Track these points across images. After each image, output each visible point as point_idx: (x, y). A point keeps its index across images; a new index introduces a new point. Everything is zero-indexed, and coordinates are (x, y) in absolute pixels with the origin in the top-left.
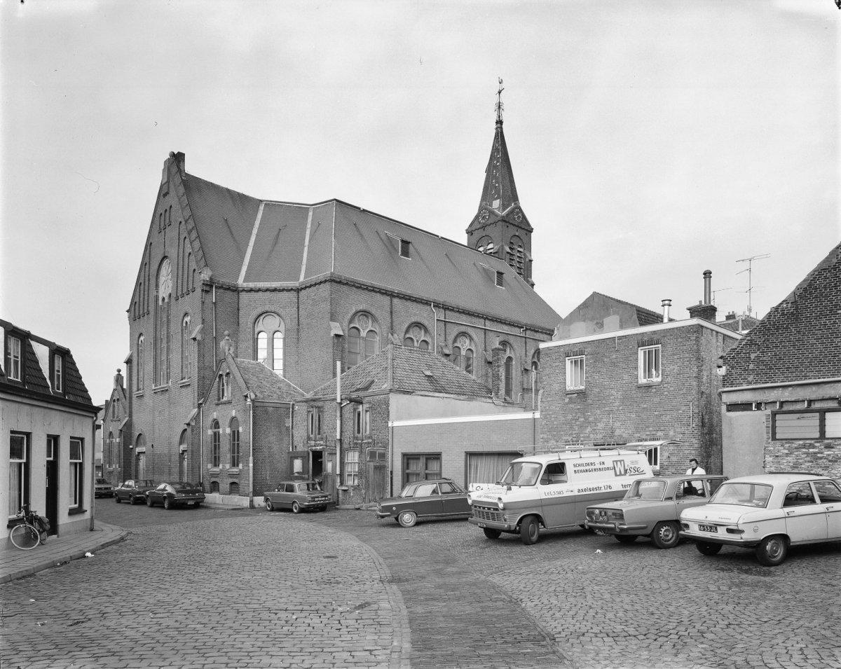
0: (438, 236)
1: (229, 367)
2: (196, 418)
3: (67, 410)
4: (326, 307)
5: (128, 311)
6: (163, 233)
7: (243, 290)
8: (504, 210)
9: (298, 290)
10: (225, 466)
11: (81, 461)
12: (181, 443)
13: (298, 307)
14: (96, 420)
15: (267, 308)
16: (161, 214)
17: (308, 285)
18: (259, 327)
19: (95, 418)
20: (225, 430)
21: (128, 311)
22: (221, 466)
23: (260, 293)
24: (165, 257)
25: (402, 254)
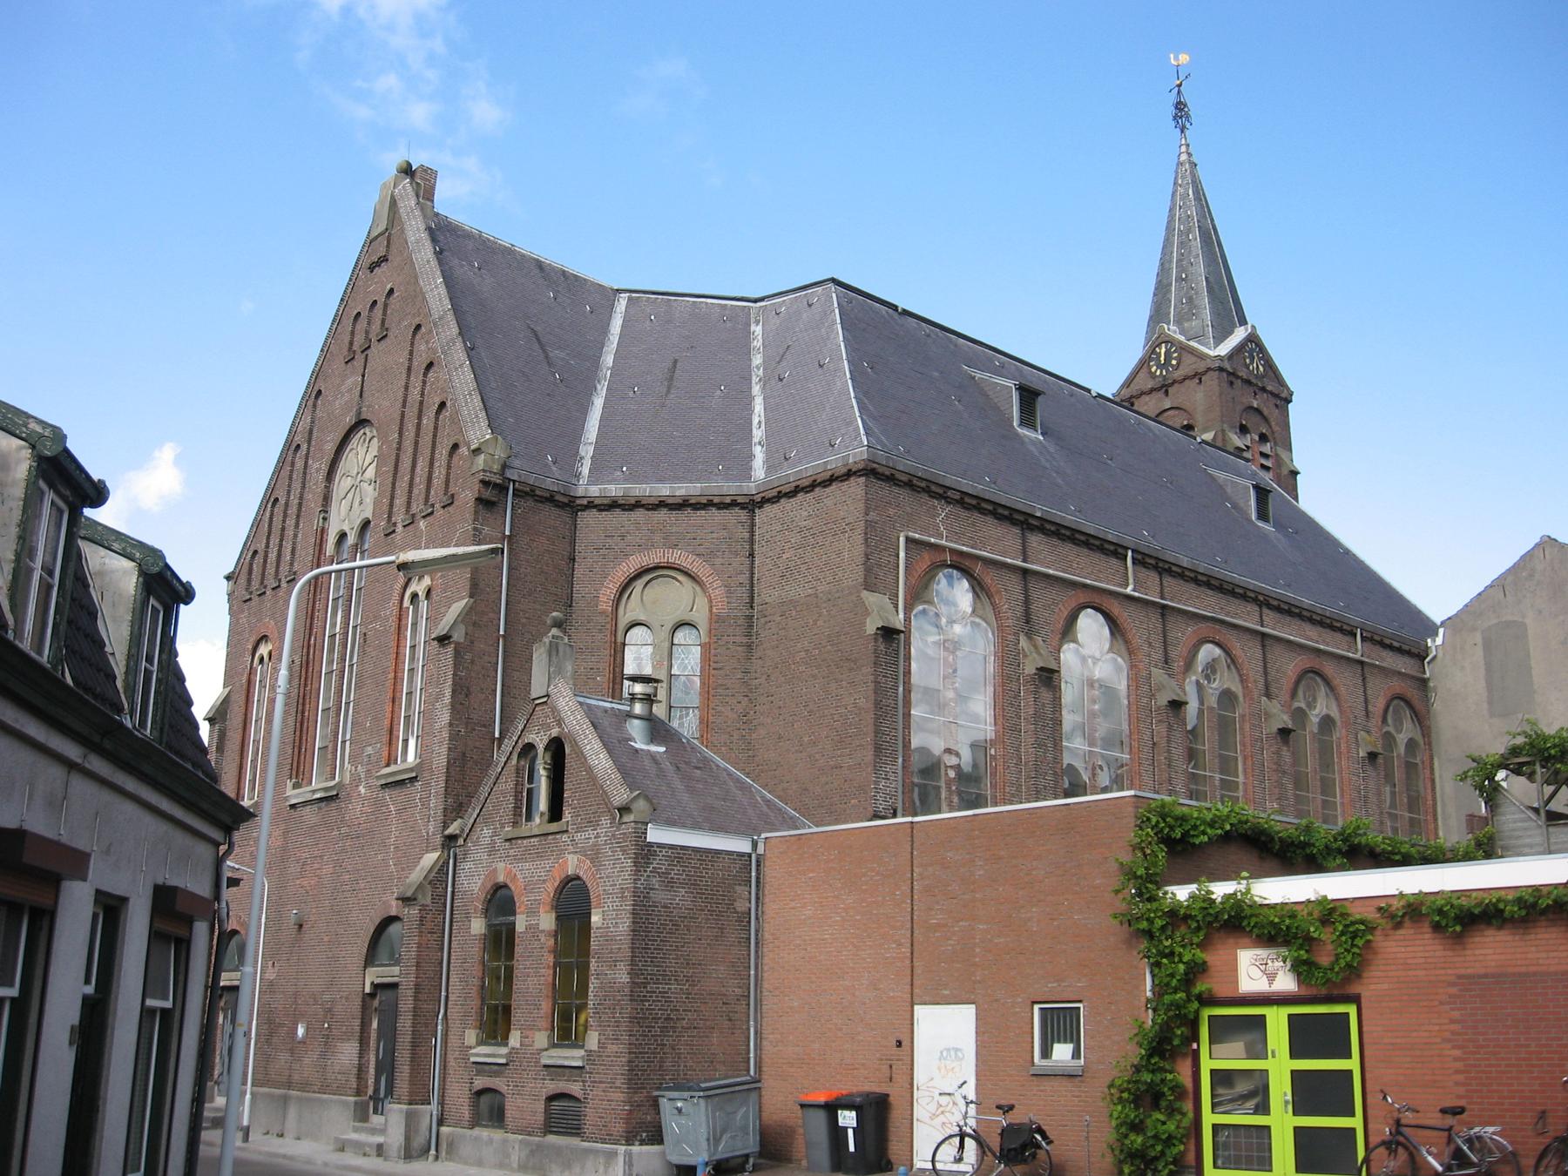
0: (1089, 391)
1: (560, 722)
2: (439, 876)
3: (165, 805)
4: (851, 548)
5: (228, 578)
6: (360, 358)
7: (591, 505)
8: (1220, 338)
9: (752, 505)
10: (531, 1036)
11: (168, 1004)
12: (370, 959)
13: (752, 555)
14: (228, 853)
15: (676, 556)
16: (375, 302)
17: (786, 489)
18: (632, 609)
19: (223, 848)
20: (536, 921)
21: (228, 578)
22: (515, 1040)
23: (639, 514)
24: (361, 423)
25: (1022, 424)
